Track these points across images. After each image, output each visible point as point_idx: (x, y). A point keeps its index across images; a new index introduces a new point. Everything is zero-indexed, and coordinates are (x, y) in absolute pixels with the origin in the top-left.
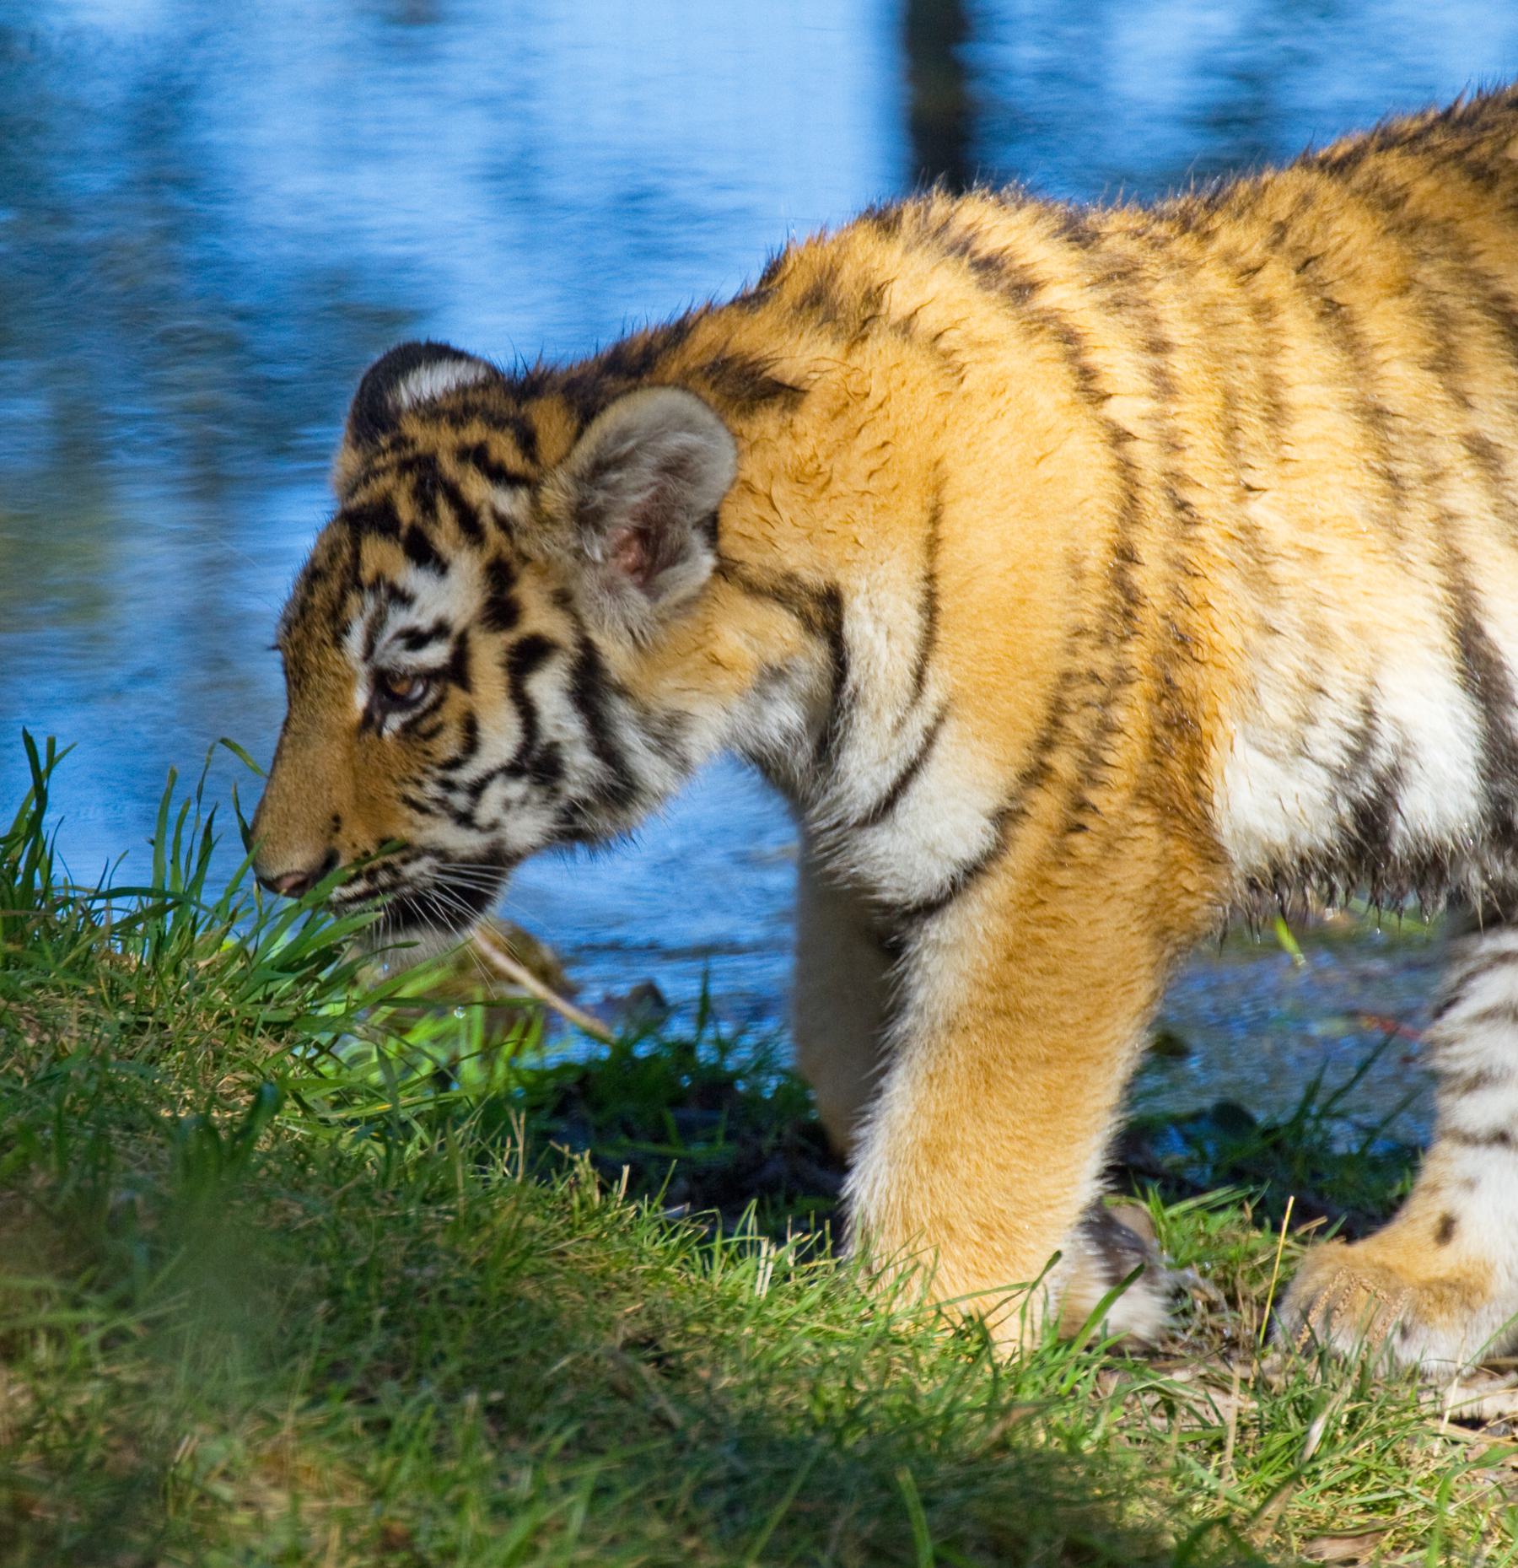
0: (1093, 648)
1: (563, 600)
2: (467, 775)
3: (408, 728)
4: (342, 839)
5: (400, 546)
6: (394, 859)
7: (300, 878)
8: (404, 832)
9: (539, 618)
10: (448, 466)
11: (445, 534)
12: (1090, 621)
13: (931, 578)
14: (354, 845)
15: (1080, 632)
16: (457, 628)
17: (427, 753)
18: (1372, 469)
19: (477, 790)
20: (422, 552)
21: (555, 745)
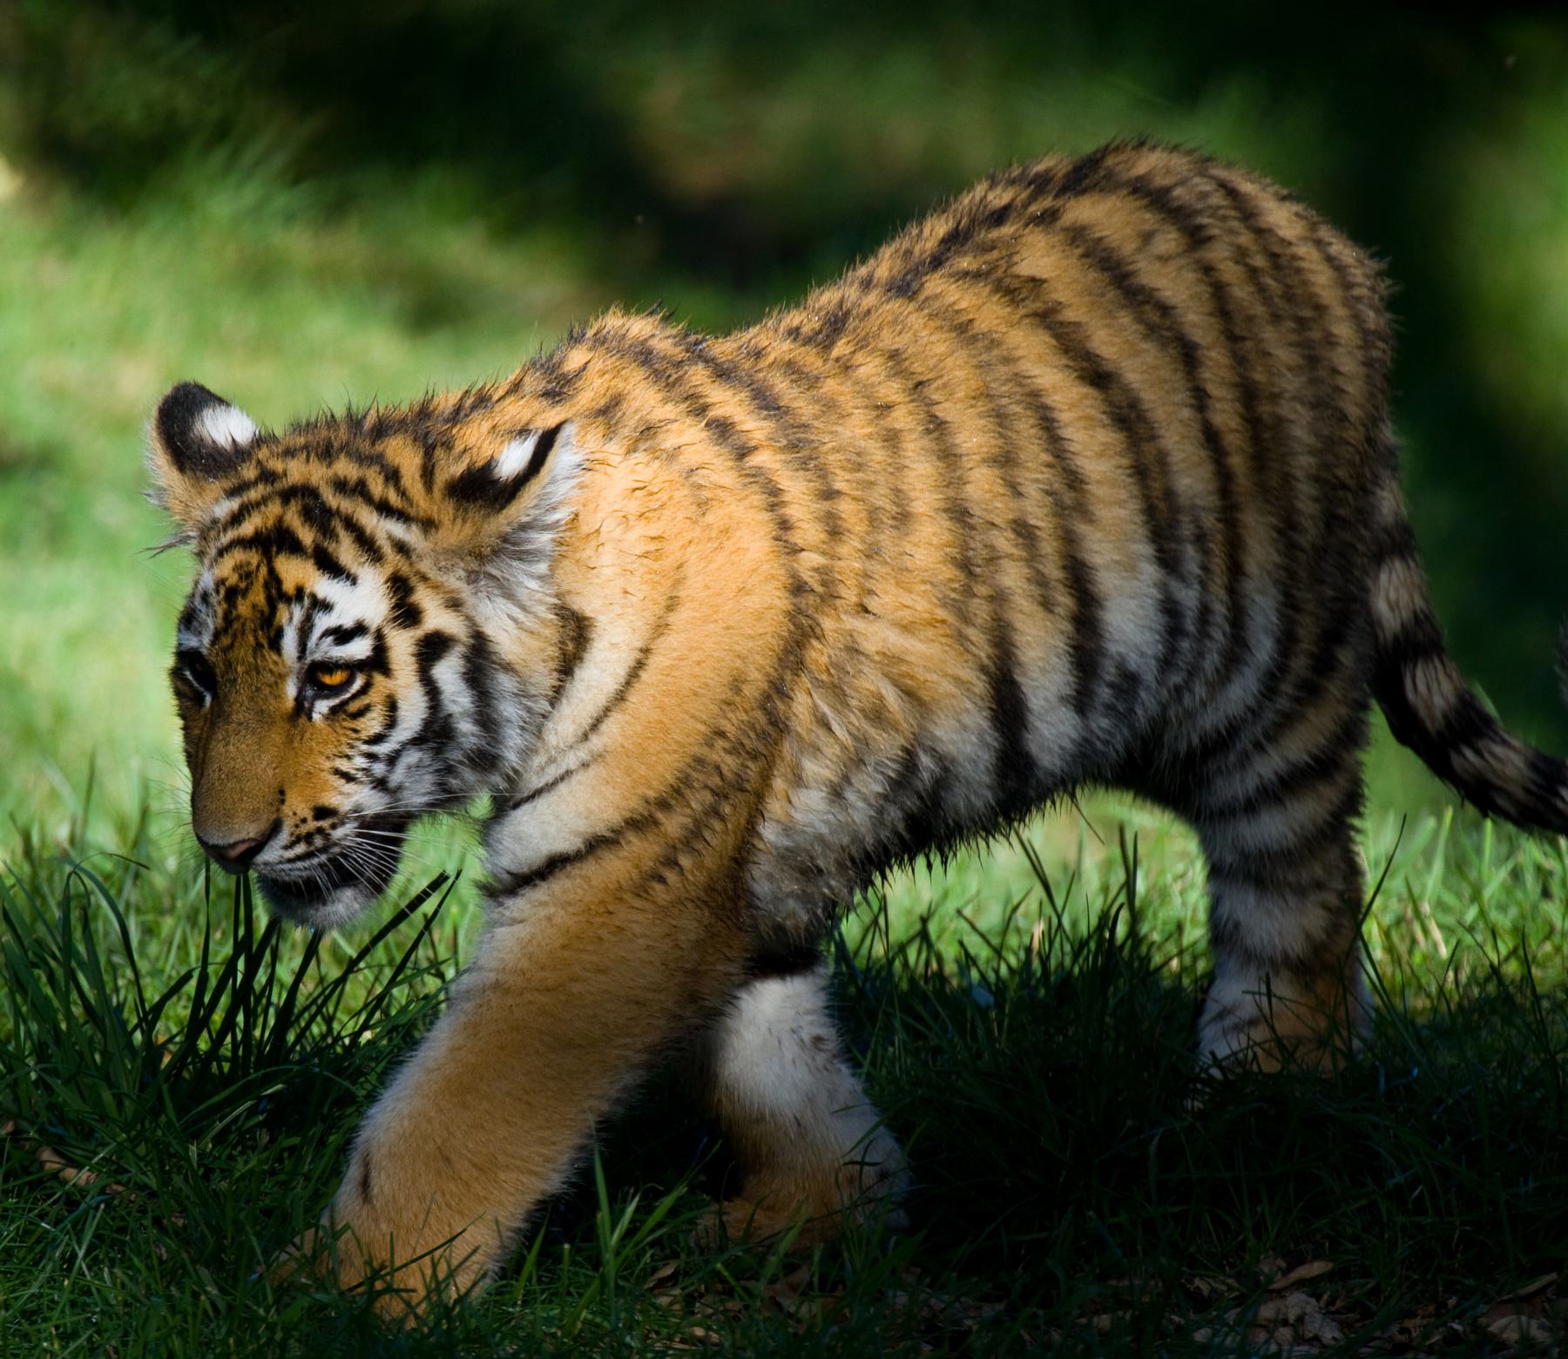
0: (724, 749)
1: (454, 604)
2: (382, 749)
3: (334, 710)
6: (325, 824)
7: (253, 844)
8: (332, 800)
9: (437, 618)
10: (332, 499)
11: (346, 551)
13: (646, 651)
14: (295, 814)
15: (721, 734)
16: (373, 628)
17: (355, 731)
19: (392, 760)
20: (330, 566)
21: (450, 715)
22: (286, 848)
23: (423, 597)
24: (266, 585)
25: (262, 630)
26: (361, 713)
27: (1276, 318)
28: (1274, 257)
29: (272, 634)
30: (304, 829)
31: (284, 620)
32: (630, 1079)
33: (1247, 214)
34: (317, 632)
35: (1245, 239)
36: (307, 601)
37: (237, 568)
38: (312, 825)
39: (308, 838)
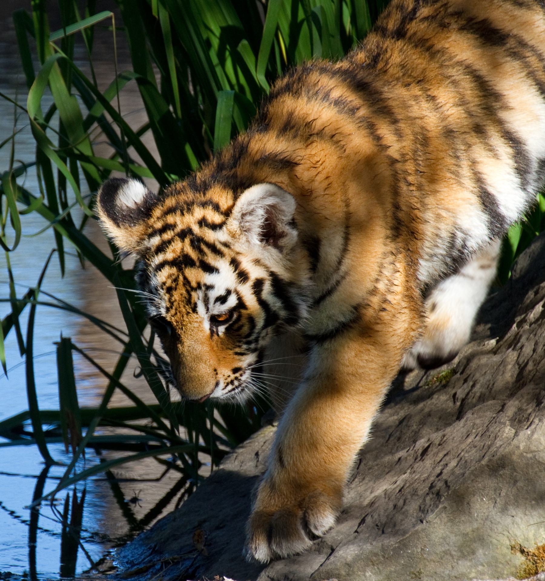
4: (220, 376)
5: (200, 269)
6: (237, 375)
14: (224, 375)
18: (470, 236)
20: (210, 269)
22: (223, 389)
24: (184, 285)
25: (187, 305)
29: (193, 306)
30: (229, 380)
31: (196, 299)
32: (389, 388)
34: (212, 300)
36: (203, 288)
37: (170, 276)
38: (233, 376)
39: (232, 382)
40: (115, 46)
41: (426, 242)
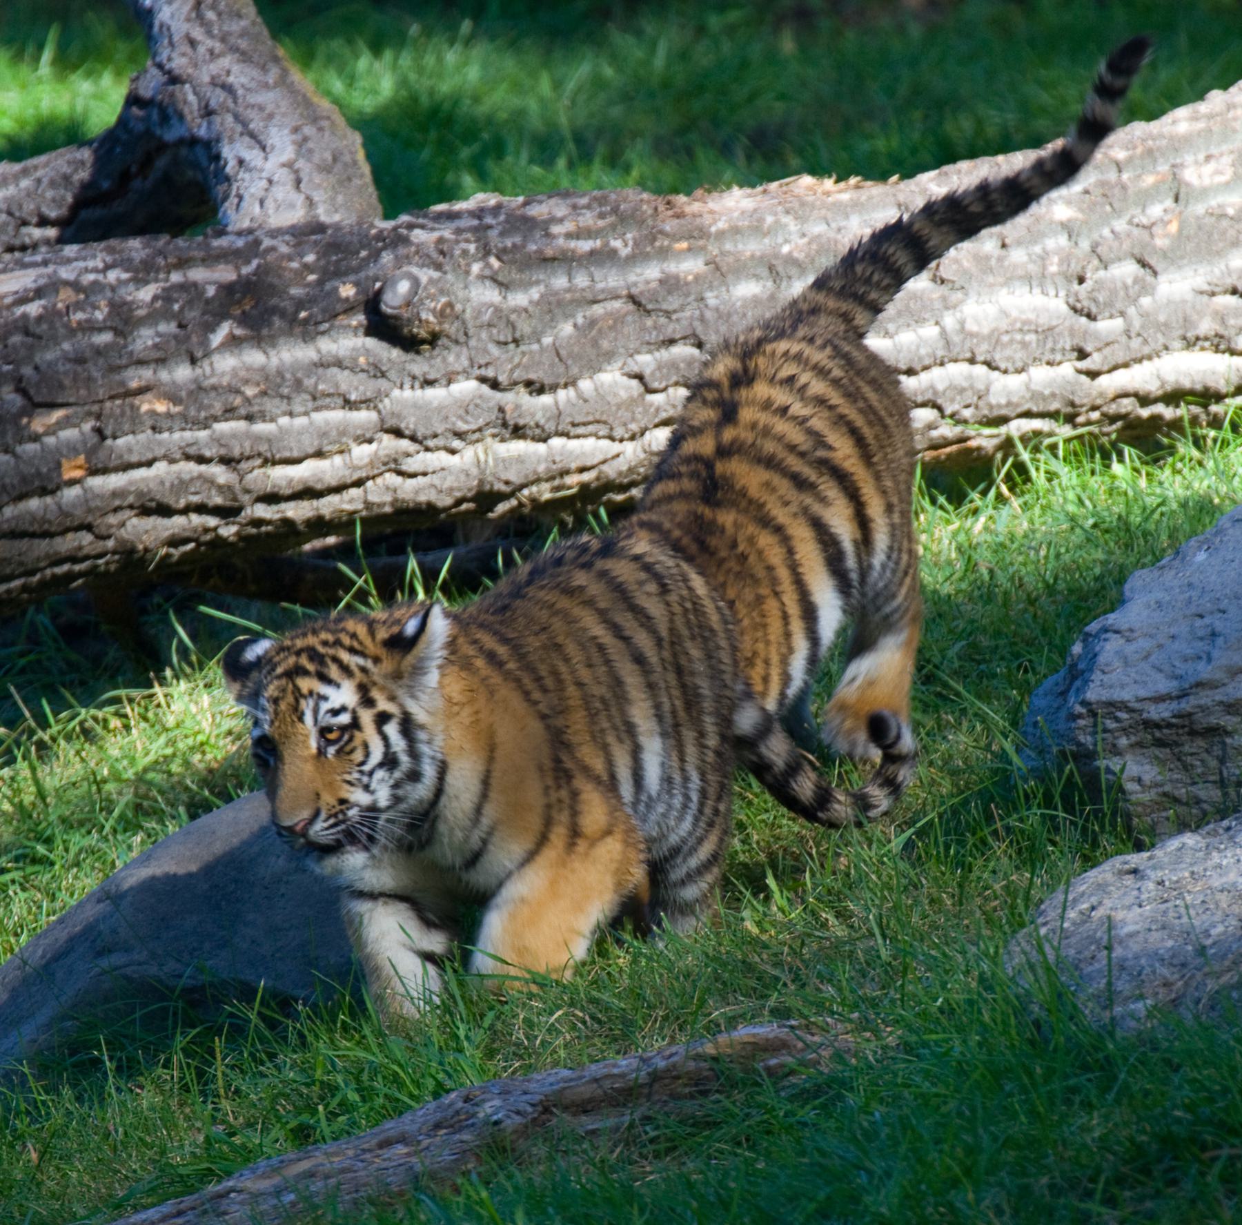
1: (392, 698)
2: (367, 768)
3: (339, 752)
8: (344, 795)
10: (321, 649)
11: (334, 672)
12: (1117, 483)
19: (371, 774)
20: (325, 679)
23: (375, 694)
26: (352, 751)
27: (693, 638)
28: (694, 603)
33: (686, 580)
35: (685, 592)
37: (278, 688)
38: (338, 808)
39: (335, 815)
40: (17, 697)
41: (836, 806)
